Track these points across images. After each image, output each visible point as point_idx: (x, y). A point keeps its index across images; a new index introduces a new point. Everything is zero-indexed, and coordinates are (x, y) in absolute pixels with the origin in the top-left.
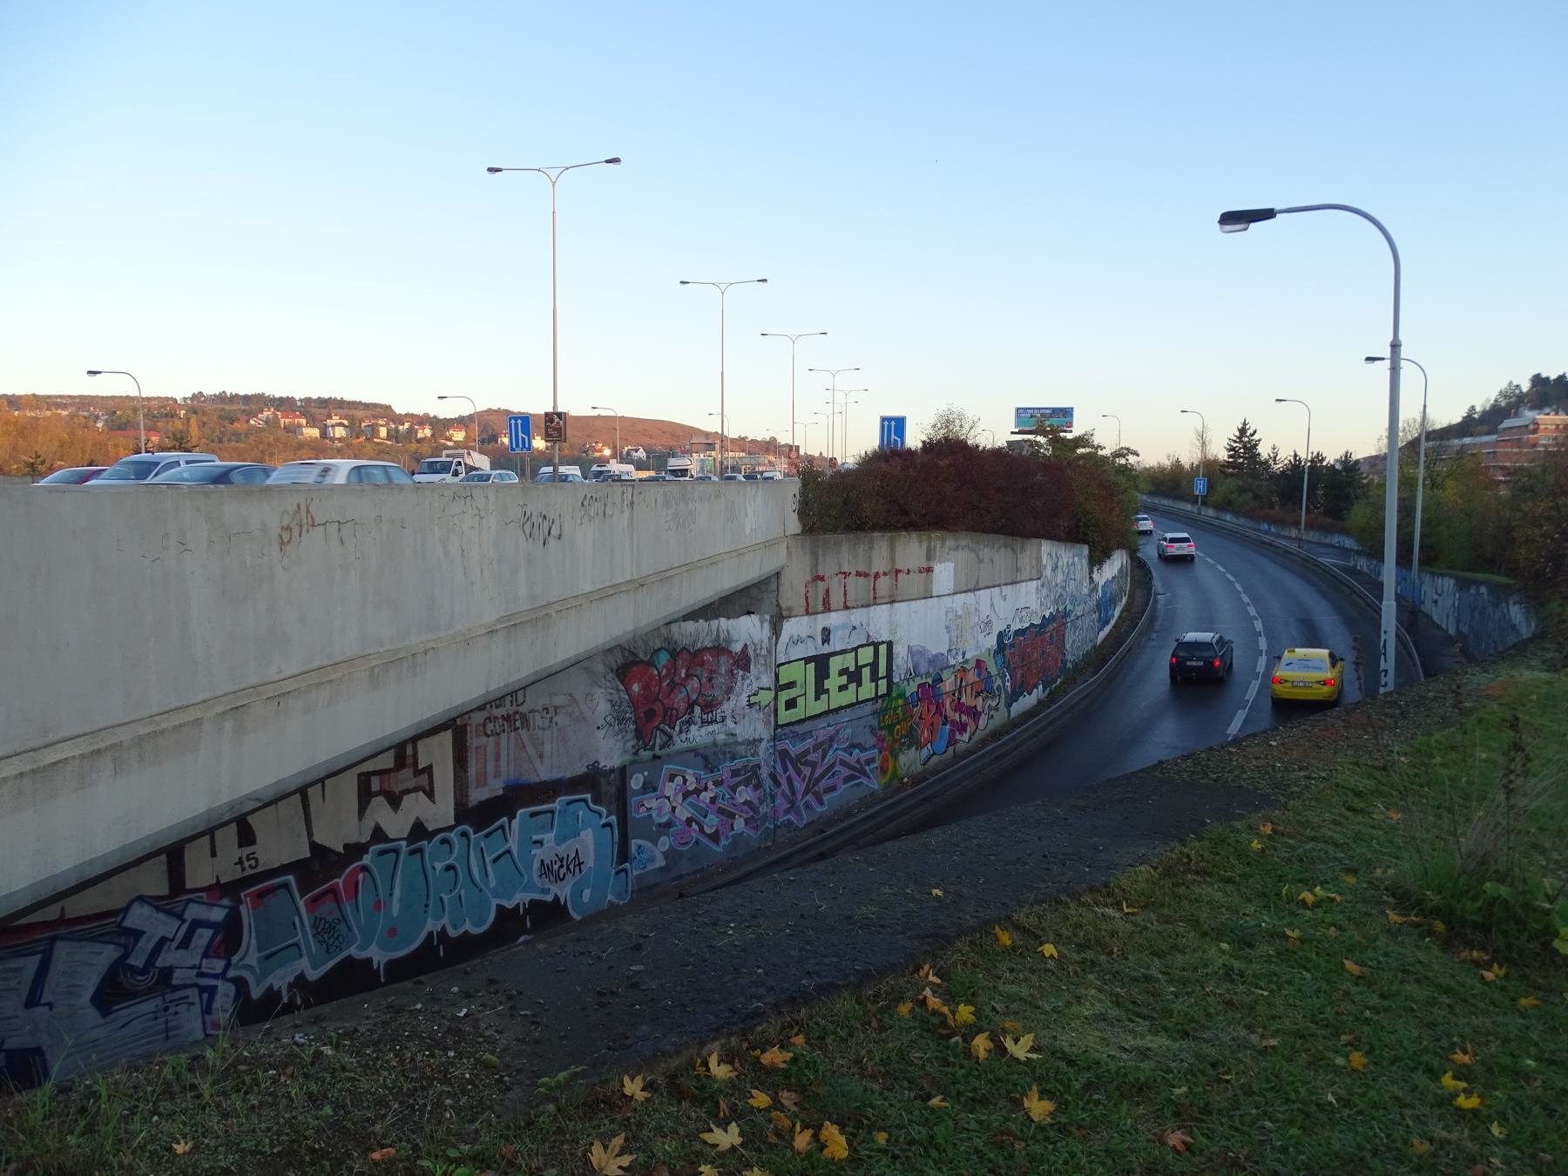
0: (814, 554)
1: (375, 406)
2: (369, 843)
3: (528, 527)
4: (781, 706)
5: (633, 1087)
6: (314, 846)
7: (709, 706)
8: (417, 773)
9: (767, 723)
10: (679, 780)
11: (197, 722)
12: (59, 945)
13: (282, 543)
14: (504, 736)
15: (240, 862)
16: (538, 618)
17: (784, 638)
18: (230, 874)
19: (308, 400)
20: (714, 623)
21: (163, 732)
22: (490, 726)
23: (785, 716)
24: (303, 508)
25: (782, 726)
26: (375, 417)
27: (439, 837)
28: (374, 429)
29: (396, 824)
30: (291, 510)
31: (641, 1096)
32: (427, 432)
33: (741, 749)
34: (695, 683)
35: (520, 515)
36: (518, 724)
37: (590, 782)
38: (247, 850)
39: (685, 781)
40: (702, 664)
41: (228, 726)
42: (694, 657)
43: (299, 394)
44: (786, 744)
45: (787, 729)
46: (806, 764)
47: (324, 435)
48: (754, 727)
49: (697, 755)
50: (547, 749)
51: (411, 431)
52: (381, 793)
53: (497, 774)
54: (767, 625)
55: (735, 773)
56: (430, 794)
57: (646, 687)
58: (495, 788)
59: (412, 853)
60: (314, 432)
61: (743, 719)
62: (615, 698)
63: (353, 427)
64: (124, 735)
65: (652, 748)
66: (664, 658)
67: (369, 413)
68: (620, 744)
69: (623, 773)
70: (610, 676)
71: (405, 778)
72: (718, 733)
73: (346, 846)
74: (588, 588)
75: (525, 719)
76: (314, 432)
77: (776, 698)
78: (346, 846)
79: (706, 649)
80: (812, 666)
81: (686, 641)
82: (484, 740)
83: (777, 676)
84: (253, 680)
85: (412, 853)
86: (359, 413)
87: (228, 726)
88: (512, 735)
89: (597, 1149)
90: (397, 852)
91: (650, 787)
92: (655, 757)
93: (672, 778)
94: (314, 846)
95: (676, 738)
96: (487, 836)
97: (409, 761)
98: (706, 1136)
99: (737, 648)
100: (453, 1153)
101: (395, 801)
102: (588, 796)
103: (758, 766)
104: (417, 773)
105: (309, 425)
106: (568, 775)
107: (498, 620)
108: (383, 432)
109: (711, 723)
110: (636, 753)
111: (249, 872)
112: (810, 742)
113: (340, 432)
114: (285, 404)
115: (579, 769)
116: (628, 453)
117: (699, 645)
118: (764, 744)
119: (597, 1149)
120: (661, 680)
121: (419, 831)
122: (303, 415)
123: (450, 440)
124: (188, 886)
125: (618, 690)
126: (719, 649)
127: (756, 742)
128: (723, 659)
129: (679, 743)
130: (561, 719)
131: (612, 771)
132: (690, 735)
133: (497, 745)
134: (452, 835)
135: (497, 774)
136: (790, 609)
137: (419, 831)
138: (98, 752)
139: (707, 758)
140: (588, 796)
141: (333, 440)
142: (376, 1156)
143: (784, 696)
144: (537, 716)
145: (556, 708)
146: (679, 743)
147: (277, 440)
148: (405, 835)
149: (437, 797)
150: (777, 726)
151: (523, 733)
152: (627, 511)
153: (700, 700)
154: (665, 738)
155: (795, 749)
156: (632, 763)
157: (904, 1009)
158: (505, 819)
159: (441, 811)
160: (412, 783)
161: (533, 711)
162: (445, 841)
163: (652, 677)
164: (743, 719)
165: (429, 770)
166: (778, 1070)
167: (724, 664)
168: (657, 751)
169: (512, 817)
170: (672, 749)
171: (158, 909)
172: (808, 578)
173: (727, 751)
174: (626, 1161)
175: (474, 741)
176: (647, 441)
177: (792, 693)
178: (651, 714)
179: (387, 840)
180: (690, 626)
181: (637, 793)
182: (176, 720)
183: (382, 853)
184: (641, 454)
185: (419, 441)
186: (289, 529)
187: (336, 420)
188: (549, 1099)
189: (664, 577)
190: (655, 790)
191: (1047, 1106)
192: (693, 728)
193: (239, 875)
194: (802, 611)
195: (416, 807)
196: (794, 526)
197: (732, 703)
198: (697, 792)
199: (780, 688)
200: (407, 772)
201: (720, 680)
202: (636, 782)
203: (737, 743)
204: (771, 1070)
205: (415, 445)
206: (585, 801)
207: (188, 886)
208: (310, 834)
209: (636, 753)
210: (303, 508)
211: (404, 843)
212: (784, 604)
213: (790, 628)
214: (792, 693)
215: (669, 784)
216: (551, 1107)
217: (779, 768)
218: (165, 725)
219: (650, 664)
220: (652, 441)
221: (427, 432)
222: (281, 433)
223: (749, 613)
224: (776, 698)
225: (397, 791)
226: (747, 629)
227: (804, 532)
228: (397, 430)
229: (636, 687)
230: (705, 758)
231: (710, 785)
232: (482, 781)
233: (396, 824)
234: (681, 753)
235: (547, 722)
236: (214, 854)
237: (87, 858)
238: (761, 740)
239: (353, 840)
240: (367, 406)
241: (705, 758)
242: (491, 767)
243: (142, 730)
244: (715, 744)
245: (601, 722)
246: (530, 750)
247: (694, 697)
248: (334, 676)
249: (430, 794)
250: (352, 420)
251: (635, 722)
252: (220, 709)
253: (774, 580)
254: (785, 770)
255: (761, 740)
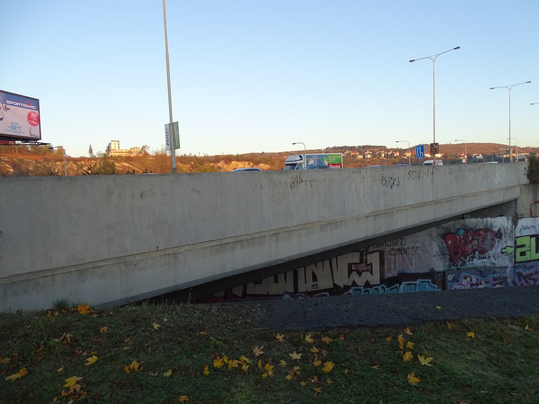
0: (535, 192)
1: (380, 147)
2: (351, 286)
3: (384, 182)
4: (518, 254)
5: (280, 337)
6: (334, 284)
7: (482, 252)
8: (367, 265)
9: (510, 261)
10: (469, 279)
11: (264, 236)
12: (233, 292)
13: (292, 187)
14: (397, 256)
15: (313, 286)
16: (389, 212)
17: (519, 226)
18: (310, 289)
19: (359, 147)
20: (485, 220)
21: (254, 238)
22: (392, 252)
23: (519, 258)
24: (298, 177)
25: (518, 262)
26: (381, 150)
27: (375, 287)
28: (380, 154)
29: (360, 281)
30: (295, 177)
31: (281, 340)
32: (398, 154)
33: (498, 270)
34: (476, 242)
35: (380, 177)
36: (403, 252)
37: (431, 275)
38: (315, 283)
39: (471, 280)
40: (479, 235)
41: (274, 238)
42: (476, 232)
43: (356, 145)
44: (521, 270)
45: (521, 264)
46: (531, 279)
47: (364, 157)
48: (504, 262)
49: (477, 270)
50: (414, 262)
51: (392, 154)
52: (355, 270)
53: (395, 269)
54: (510, 221)
55: (495, 279)
56: (371, 273)
57: (454, 242)
58: (394, 273)
59: (365, 291)
60: (361, 157)
61: (499, 257)
62: (441, 246)
63: (374, 155)
64: (244, 238)
65: (457, 266)
66: (462, 232)
67: (378, 149)
68: (443, 263)
69: (444, 273)
70: (439, 237)
71: (363, 267)
72: (486, 262)
73: (344, 286)
74: (411, 203)
75: (405, 250)
76: (361, 157)
77: (515, 251)
78: (344, 286)
79: (481, 229)
80: (534, 239)
81: (472, 226)
82: (390, 256)
83: (515, 242)
84: (282, 226)
85: (365, 291)
86: (375, 150)
87: (274, 238)
88: (400, 256)
89: (257, 348)
90: (360, 290)
91: (455, 280)
92: (458, 269)
93: (465, 278)
94: (334, 284)
95: (467, 263)
96: (391, 289)
97: (364, 261)
98: (291, 355)
99: (496, 229)
100: (219, 338)
101: (360, 274)
102: (430, 280)
103: (506, 278)
104: (367, 265)
105: (360, 155)
106: (422, 272)
107: (372, 213)
108: (383, 155)
109: (483, 258)
110: (450, 267)
111: (315, 289)
112: (533, 270)
113: (369, 156)
114: (352, 149)
115: (426, 270)
116: (475, 157)
117: (478, 228)
118: (509, 269)
119: (257, 348)
120: (461, 240)
121: (367, 285)
122: (358, 151)
123: (406, 156)
124: (299, 291)
125: (442, 243)
126: (487, 229)
127: (505, 268)
128: (489, 234)
129: (469, 265)
130: (419, 252)
131: (440, 272)
132: (474, 262)
133: (395, 259)
134: (379, 287)
135: (395, 269)
136: (522, 215)
137: (367, 285)
138: (237, 242)
139: (482, 272)
140: (430, 280)
141: (367, 159)
142: (202, 333)
143: (519, 250)
144: (410, 250)
145: (417, 247)
146: (469, 265)
147: (350, 160)
148: (363, 285)
149: (374, 274)
150: (515, 262)
151: (405, 255)
152: (430, 176)
153: (478, 249)
154: (462, 262)
155: (525, 273)
156: (448, 270)
157: (389, 339)
158: (398, 285)
159: (375, 279)
160: (365, 268)
161: (408, 248)
162: (376, 289)
163: (457, 239)
164: (499, 257)
165: (371, 265)
166: (326, 344)
167: (489, 236)
168: (459, 267)
169: (400, 284)
170: (465, 267)
171: (291, 296)
172: (532, 202)
173: (492, 269)
174: (261, 353)
175: (387, 257)
176: (484, 152)
177: (523, 249)
178: (456, 253)
179: (357, 286)
180: (473, 221)
181: (450, 282)
182: (258, 235)
183: (355, 290)
184: (481, 156)
185: (395, 157)
186: (294, 182)
187: (368, 152)
188: (253, 333)
189: (449, 200)
190: (458, 281)
191: (417, 380)
192: (475, 260)
193: (313, 290)
194: (528, 215)
195: (366, 276)
196: (525, 180)
197: (493, 251)
198: (477, 284)
199: (516, 247)
200: (364, 265)
201: (488, 242)
202: (450, 277)
203: (495, 267)
204: (324, 343)
205: (393, 159)
206: (429, 282)
207: (299, 291)
208: (333, 281)
209: (450, 267)
210: (298, 177)
211: (363, 288)
212: (519, 212)
213: (522, 223)
214: (523, 249)
215: (464, 280)
216: (253, 335)
217: (517, 279)
218: (255, 236)
219: (456, 234)
220: (485, 152)
221: (398, 154)
222: (351, 158)
223: (502, 216)
224: (515, 251)
225: (360, 270)
226: (500, 222)
227: (530, 183)
228: (387, 154)
229: (450, 242)
230: (481, 272)
231: (483, 282)
232: (389, 271)
233: (360, 281)
234: (469, 269)
235: (414, 252)
236: (306, 283)
237: (234, 269)
238: (507, 267)
239: (346, 284)
240: (378, 147)
241: (481, 272)
242: (392, 266)
243: (249, 237)
244: (485, 267)
245: (435, 254)
246: (407, 261)
247: (475, 248)
248: (308, 227)
249: (371, 273)
250: (373, 152)
251: (449, 255)
252: (271, 233)
253: (514, 203)
254: (520, 281)
255: (507, 267)
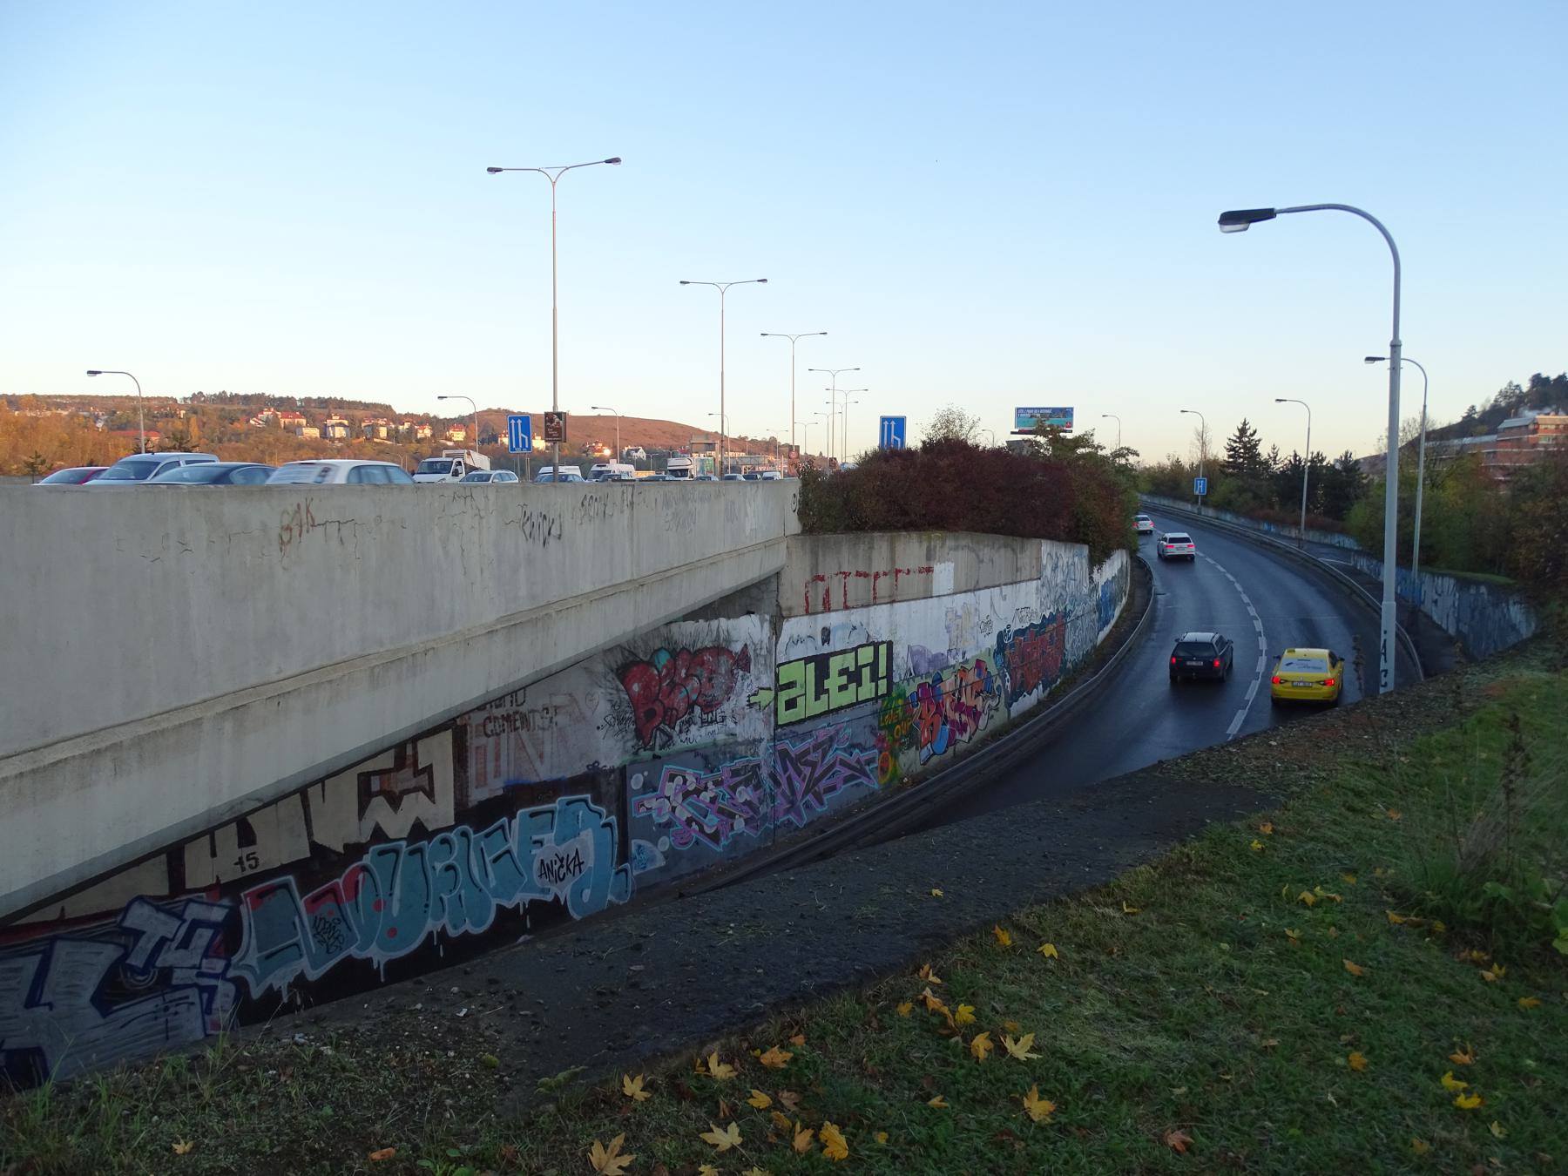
0: (814, 554)
1: (375, 406)
2: (369, 843)
3: (528, 527)
4: (781, 706)
5: (633, 1087)
6: (314, 846)
7: (709, 706)
8: (417, 773)
9: (767, 723)
10: (679, 780)
11: (197, 722)
12: (59, 945)
13: (282, 543)
14: (504, 736)
15: (240, 862)
16: (538, 618)
17: (784, 638)
18: (230, 874)
19: (308, 400)
20: (714, 623)
21: (163, 732)
22: (490, 726)
23: (785, 716)
24: (303, 508)
25: (782, 726)
26: (375, 417)
27: (439, 837)
28: (374, 429)
29: (396, 824)
30: (291, 510)
31: (641, 1096)
32: (427, 432)
33: (741, 749)
34: (695, 683)
35: (520, 515)
36: (518, 724)
37: (590, 782)
38: (247, 850)
39: (685, 781)
40: (702, 664)
41: (228, 726)
42: (694, 657)
43: (299, 394)
44: (786, 744)
45: (787, 729)
46: (806, 764)
47: (324, 435)
48: (754, 727)
49: (697, 755)
50: (547, 749)
51: (411, 431)
52: (381, 793)
53: (497, 774)
54: (767, 625)
55: (735, 773)
56: (430, 794)
57: (646, 687)
58: (495, 788)
59: (412, 853)
60: (314, 432)
61: (743, 719)
62: (615, 698)
63: (353, 427)
64: (124, 735)
65: (652, 748)
66: (664, 658)
67: (369, 413)
68: (620, 744)
69: (623, 773)
70: (610, 676)
71: (405, 778)
72: (718, 733)
73: (346, 846)
74: (588, 588)
75: (525, 719)
76: (314, 432)
77: (776, 698)
78: (346, 846)
79: (706, 649)
80: (812, 666)
81: (686, 641)
82: (484, 740)
83: (777, 676)
84: (253, 680)
85: (412, 853)
86: (359, 413)
87: (228, 726)
88: (512, 735)
89: (597, 1149)
90: (397, 852)
91: (650, 787)
92: (655, 757)
93: (672, 778)
94: (314, 846)
95: (676, 738)
96: (487, 836)
97: (409, 761)
98: (706, 1136)
99: (737, 648)
100: (453, 1153)
101: (395, 801)
102: (588, 796)
103: (758, 766)
104: (417, 773)
105: (309, 425)
106: (568, 775)
107: (498, 620)
108: (383, 432)
109: (711, 723)
110: (636, 753)
111: (249, 872)
112: (810, 742)
113: (340, 432)
114: (285, 404)
115: (579, 769)
116: (628, 453)
117: (699, 645)
118: (764, 744)
119: (597, 1149)
120: (661, 680)
121: (419, 831)
122: (303, 415)
123: (450, 440)
124: (188, 886)
125: (618, 690)
126: (719, 649)
127: (756, 742)
128: (723, 659)
129: (679, 743)
130: (561, 719)
131: (612, 771)
132: (690, 735)
133: (497, 745)
134: (452, 835)
135: (497, 774)
136: (790, 609)
137: (419, 831)
138: (98, 752)
139: (707, 758)
140: (588, 796)
141: (333, 440)
142: (376, 1156)
143: (784, 696)
144: (537, 716)
145: (556, 708)
146: (679, 743)
147: (277, 440)
148: (405, 835)
149: (437, 797)
150: (777, 726)
151: (523, 733)
152: (627, 511)
153: (700, 700)
154: (665, 738)
155: (795, 749)
156: (632, 763)
157: (904, 1009)
158: (505, 819)
159: (441, 811)
160: (412, 783)
161: (533, 711)
162: (445, 841)
163: (652, 677)
164: (743, 719)
165: (429, 770)
166: (778, 1070)
167: (724, 664)
168: (657, 751)
169: (512, 817)
170: (672, 749)
171: (158, 909)
172: (808, 578)
173: (727, 751)
174: (626, 1161)
175: (474, 741)
176: (647, 441)
177: (792, 693)
178: (651, 714)
179: (387, 840)
180: (690, 626)
181: (637, 793)
182: (176, 720)
183: (382, 853)
184: (641, 454)
185: (419, 441)
186: (289, 529)
187: (336, 420)
188: (549, 1099)
189: (664, 577)
190: (655, 790)
191: (1047, 1106)
192: (693, 728)
193: (239, 875)
194: (802, 611)
195: (416, 807)
196: (794, 526)
197: (732, 703)
198: (697, 792)
199: (780, 688)
200: (407, 772)
201: (720, 680)
202: (636, 782)
203: (737, 743)
204: (771, 1070)
205: (415, 445)
206: (585, 801)
207: (188, 886)
208: (310, 834)
209: (636, 753)
210: (303, 508)
211: (404, 843)
212: (784, 604)
213: (790, 628)
214: (792, 693)
215: (669, 784)
216: (551, 1107)
217: (779, 768)
218: (165, 725)
219: (650, 664)
220: (652, 441)
221: (427, 432)
222: (281, 433)
223: (749, 613)
224: (776, 698)
225: (397, 791)
226: (747, 629)
227: (804, 532)
228: (397, 430)
229: (636, 687)
230: (705, 758)
231: (710, 785)
232: (482, 781)
233: (396, 824)
234: (681, 753)
235: (547, 722)
236: (214, 854)
237: (87, 858)
238: (761, 740)
239: (353, 840)
240: (367, 406)
241: (705, 758)
242: (491, 767)
243: (142, 730)
244: (715, 744)
245: (601, 722)
246: (530, 750)
247: (694, 697)
248: (334, 676)
249: (430, 794)
250: (352, 420)
251: (635, 722)
252: (220, 709)
253: (774, 580)
254: (785, 770)
255: (761, 740)
